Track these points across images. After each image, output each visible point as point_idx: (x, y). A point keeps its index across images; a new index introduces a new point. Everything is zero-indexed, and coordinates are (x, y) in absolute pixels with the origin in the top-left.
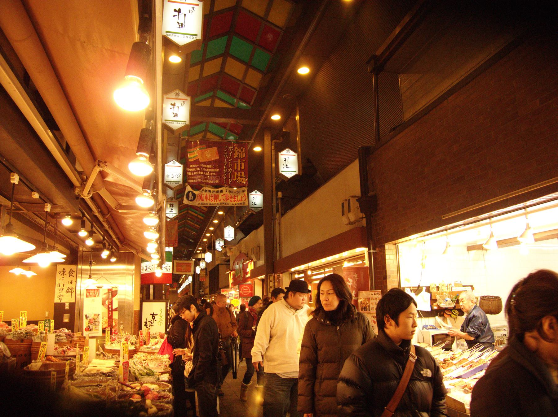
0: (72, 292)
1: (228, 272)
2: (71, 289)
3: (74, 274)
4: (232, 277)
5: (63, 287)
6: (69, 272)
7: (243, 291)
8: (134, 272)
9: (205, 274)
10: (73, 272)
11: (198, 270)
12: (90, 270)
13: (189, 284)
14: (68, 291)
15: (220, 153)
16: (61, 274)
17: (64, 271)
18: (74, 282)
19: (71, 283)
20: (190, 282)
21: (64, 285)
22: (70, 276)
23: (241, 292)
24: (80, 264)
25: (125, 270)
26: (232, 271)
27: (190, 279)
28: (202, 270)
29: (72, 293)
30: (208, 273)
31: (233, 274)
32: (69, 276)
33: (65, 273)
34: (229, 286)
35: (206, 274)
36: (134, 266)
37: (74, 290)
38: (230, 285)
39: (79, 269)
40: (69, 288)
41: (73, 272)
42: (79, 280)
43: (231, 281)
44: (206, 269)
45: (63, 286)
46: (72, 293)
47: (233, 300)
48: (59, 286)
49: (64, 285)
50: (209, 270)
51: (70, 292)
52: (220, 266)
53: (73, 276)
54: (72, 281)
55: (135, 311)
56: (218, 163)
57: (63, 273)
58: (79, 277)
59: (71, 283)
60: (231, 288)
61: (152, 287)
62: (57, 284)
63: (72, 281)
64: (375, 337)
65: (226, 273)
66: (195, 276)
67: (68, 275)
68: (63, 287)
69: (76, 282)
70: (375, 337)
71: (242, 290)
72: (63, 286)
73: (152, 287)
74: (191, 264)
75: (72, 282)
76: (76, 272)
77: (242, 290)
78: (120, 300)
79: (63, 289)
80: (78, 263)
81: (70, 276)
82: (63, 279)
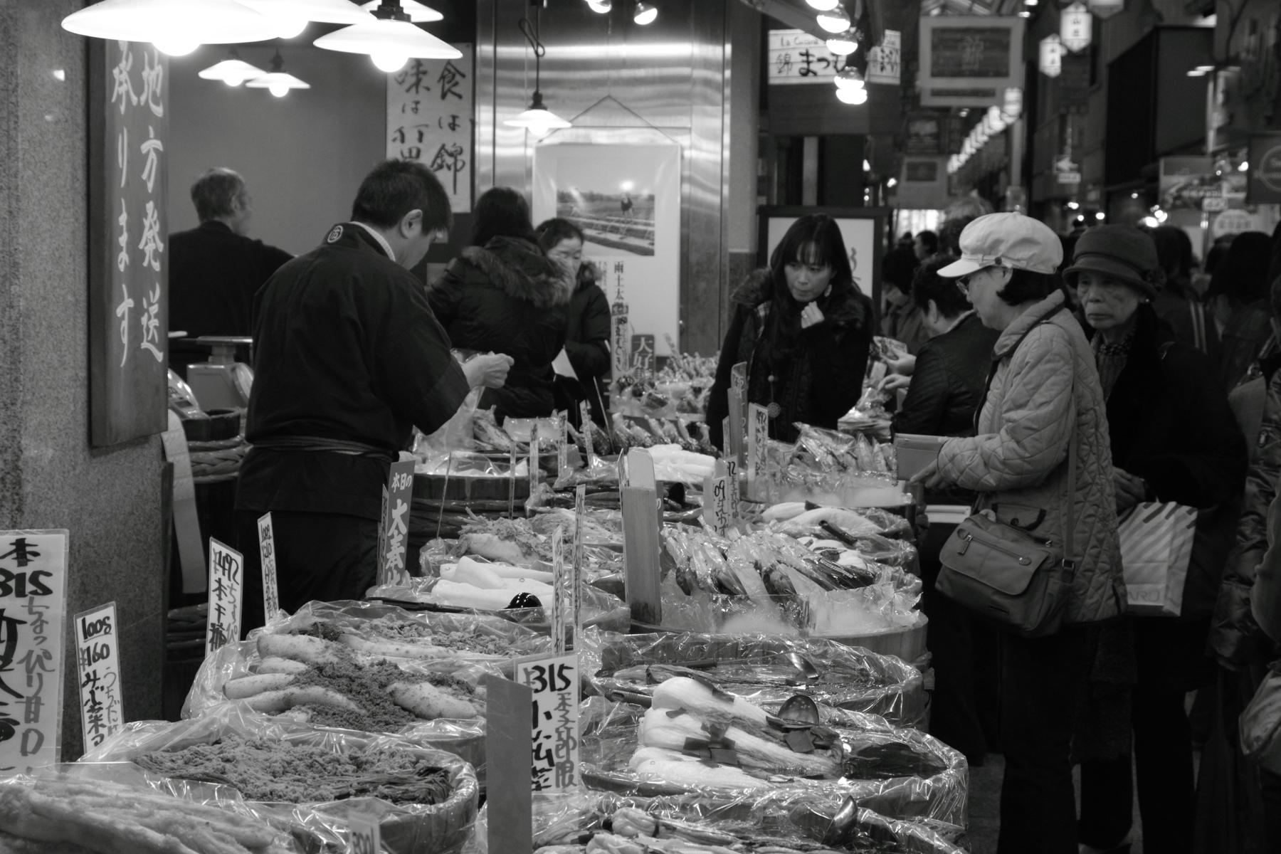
0: (459, 165)
1: (1201, 71)
2: (451, 155)
3: (464, 87)
4: (1220, 97)
5: (420, 146)
6: (443, 77)
7: (1269, 169)
8: (728, 73)
9: (1087, 76)
10: (458, 78)
11: (1051, 58)
12: (538, 64)
13: (1007, 132)
14: (439, 161)
15: (939, 126)
16: (406, 86)
17: (418, 74)
18: (464, 123)
19: (453, 126)
20: (1010, 120)
21: (421, 135)
22: (444, 96)
23: (1259, 174)
24: (486, 40)
25: (689, 62)
26: (1220, 65)
27: (1013, 98)
28: (1070, 58)
29: (456, 171)
30: (1103, 73)
31: (1227, 80)
32: (439, 93)
33: (426, 81)
34: (1203, 141)
35: (1093, 80)
36: (728, 48)
37: (466, 157)
38: (1211, 135)
39: (486, 62)
40: (443, 147)
41: (458, 78)
42: (484, 114)
43: (1216, 119)
44: (1094, 48)
45: (420, 140)
46: (456, 171)
47: (1219, 218)
48: (403, 140)
49: (421, 135)
50: (1109, 54)
51: (449, 168)
52: (1165, 38)
53: (460, 97)
54: (454, 118)
55: (734, 257)
56: (936, 136)
57: (414, 80)
58: (485, 94)
59: (453, 126)
60: (1215, 154)
61: (810, 149)
62: (392, 133)
63: (454, 118)
64: (908, 235)
65: (1192, 73)
66: (1034, 80)
67: (437, 91)
68: (420, 146)
69: (473, 123)
70: (908, 235)
71: (1268, 163)
72: (420, 140)
73: (810, 149)
74: (1007, 32)
75: (457, 122)
76: (469, 76)
77: (1268, 163)
78: (693, 208)
79: (419, 151)
80: (479, 28)
81: (444, 96)
82: (416, 110)
